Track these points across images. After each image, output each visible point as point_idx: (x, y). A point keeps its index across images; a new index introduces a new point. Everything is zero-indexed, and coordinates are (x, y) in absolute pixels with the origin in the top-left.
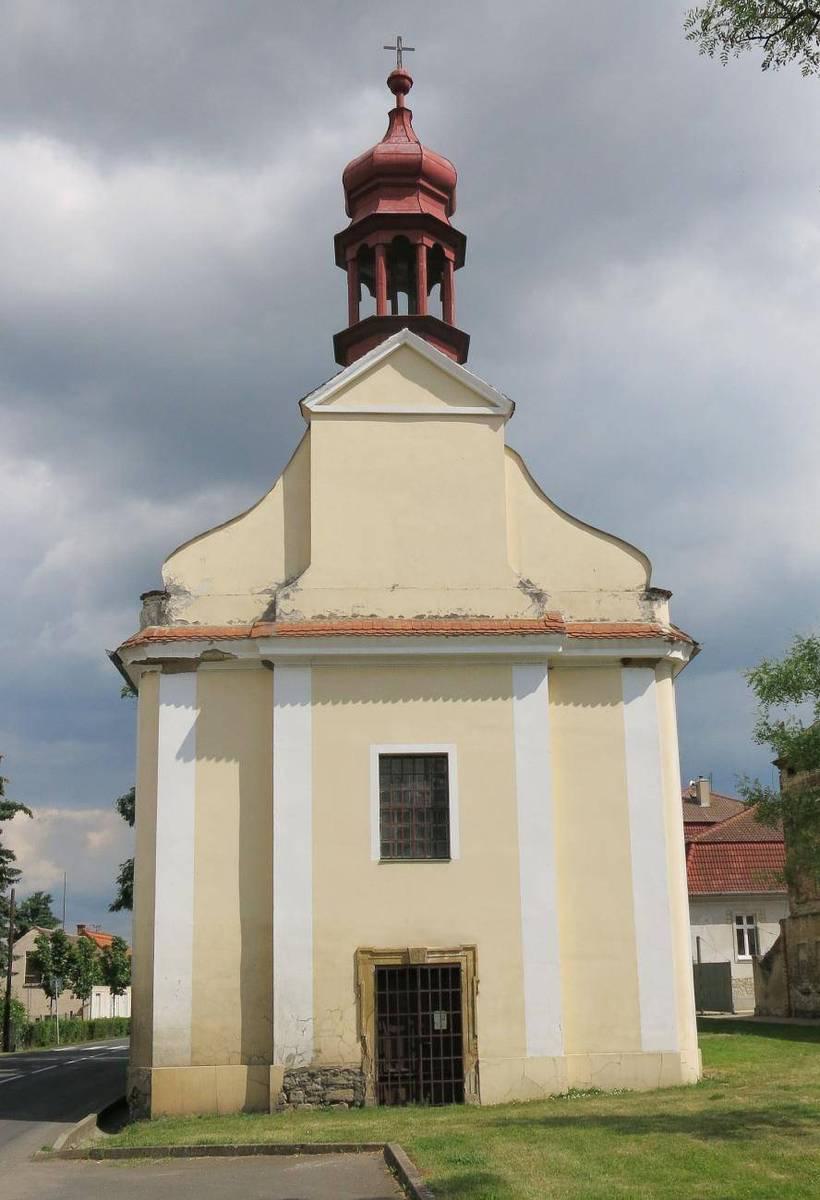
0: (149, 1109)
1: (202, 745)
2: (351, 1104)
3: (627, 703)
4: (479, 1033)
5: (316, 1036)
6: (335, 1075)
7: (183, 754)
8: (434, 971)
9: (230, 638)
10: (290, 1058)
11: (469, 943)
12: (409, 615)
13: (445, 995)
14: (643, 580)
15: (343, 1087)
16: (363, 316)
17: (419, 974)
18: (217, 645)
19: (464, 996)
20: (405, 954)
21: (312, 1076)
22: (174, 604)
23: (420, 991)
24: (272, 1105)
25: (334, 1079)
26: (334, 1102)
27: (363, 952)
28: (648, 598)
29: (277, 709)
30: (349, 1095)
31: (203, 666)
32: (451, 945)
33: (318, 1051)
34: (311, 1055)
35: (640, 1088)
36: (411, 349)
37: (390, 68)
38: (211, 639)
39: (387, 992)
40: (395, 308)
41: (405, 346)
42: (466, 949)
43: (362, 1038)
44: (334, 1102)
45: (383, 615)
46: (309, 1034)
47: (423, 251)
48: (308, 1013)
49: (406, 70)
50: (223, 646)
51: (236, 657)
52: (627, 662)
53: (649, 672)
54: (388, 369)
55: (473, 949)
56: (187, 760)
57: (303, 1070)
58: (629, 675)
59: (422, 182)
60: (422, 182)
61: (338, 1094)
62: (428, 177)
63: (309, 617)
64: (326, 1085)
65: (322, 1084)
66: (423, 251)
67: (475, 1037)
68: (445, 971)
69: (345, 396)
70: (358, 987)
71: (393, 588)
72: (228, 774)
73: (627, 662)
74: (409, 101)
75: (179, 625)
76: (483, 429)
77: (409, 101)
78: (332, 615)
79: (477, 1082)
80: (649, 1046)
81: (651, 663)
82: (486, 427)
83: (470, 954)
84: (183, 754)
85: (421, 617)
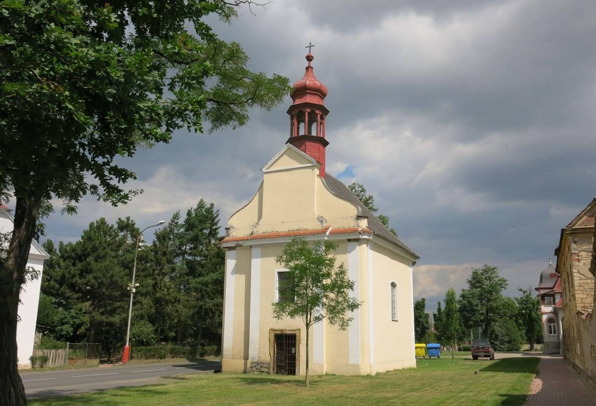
0: (44, 265)
1: (237, 271)
2: (267, 373)
3: (349, 253)
4: (300, 355)
5: (259, 353)
6: (263, 364)
7: (232, 273)
8: (289, 336)
9: (241, 240)
10: (253, 358)
11: (298, 328)
12: (286, 230)
13: (289, 340)
14: (356, 213)
15: (265, 368)
16: (300, 134)
17: (284, 337)
18: (239, 243)
19: (297, 343)
20: (282, 330)
21: (258, 364)
22: (231, 231)
23: (284, 341)
24: (247, 371)
25: (263, 365)
26: (263, 372)
27: (272, 330)
28: (357, 219)
29: (252, 260)
30: (266, 370)
31: (237, 248)
32: (294, 328)
33: (259, 357)
34: (257, 358)
35: (347, 375)
36: (291, 149)
37: (306, 53)
38: (237, 241)
39: (279, 341)
40: (310, 131)
41: (289, 148)
42: (298, 330)
43: (270, 354)
44: (263, 372)
45: (280, 231)
46: (257, 352)
47: (307, 114)
48: (257, 346)
49: (312, 54)
50: (240, 243)
51: (243, 246)
52: (349, 240)
53: (356, 243)
54: (285, 156)
55: (299, 330)
56: (234, 275)
57: (255, 362)
58: (350, 244)
59: (308, 91)
60: (308, 91)
61: (263, 369)
62: (308, 89)
63: (261, 232)
64: (261, 367)
65: (260, 366)
66: (307, 114)
67: (299, 356)
68: (292, 336)
69: (272, 167)
70: (270, 340)
71: (283, 222)
72: (242, 278)
73: (349, 240)
74: (312, 64)
75: (232, 237)
76: (310, 170)
77: (306, 63)
78: (267, 232)
79: (299, 370)
80: (351, 362)
81: (357, 240)
82: (311, 170)
83: (299, 331)
84: (232, 273)
85: (289, 231)
